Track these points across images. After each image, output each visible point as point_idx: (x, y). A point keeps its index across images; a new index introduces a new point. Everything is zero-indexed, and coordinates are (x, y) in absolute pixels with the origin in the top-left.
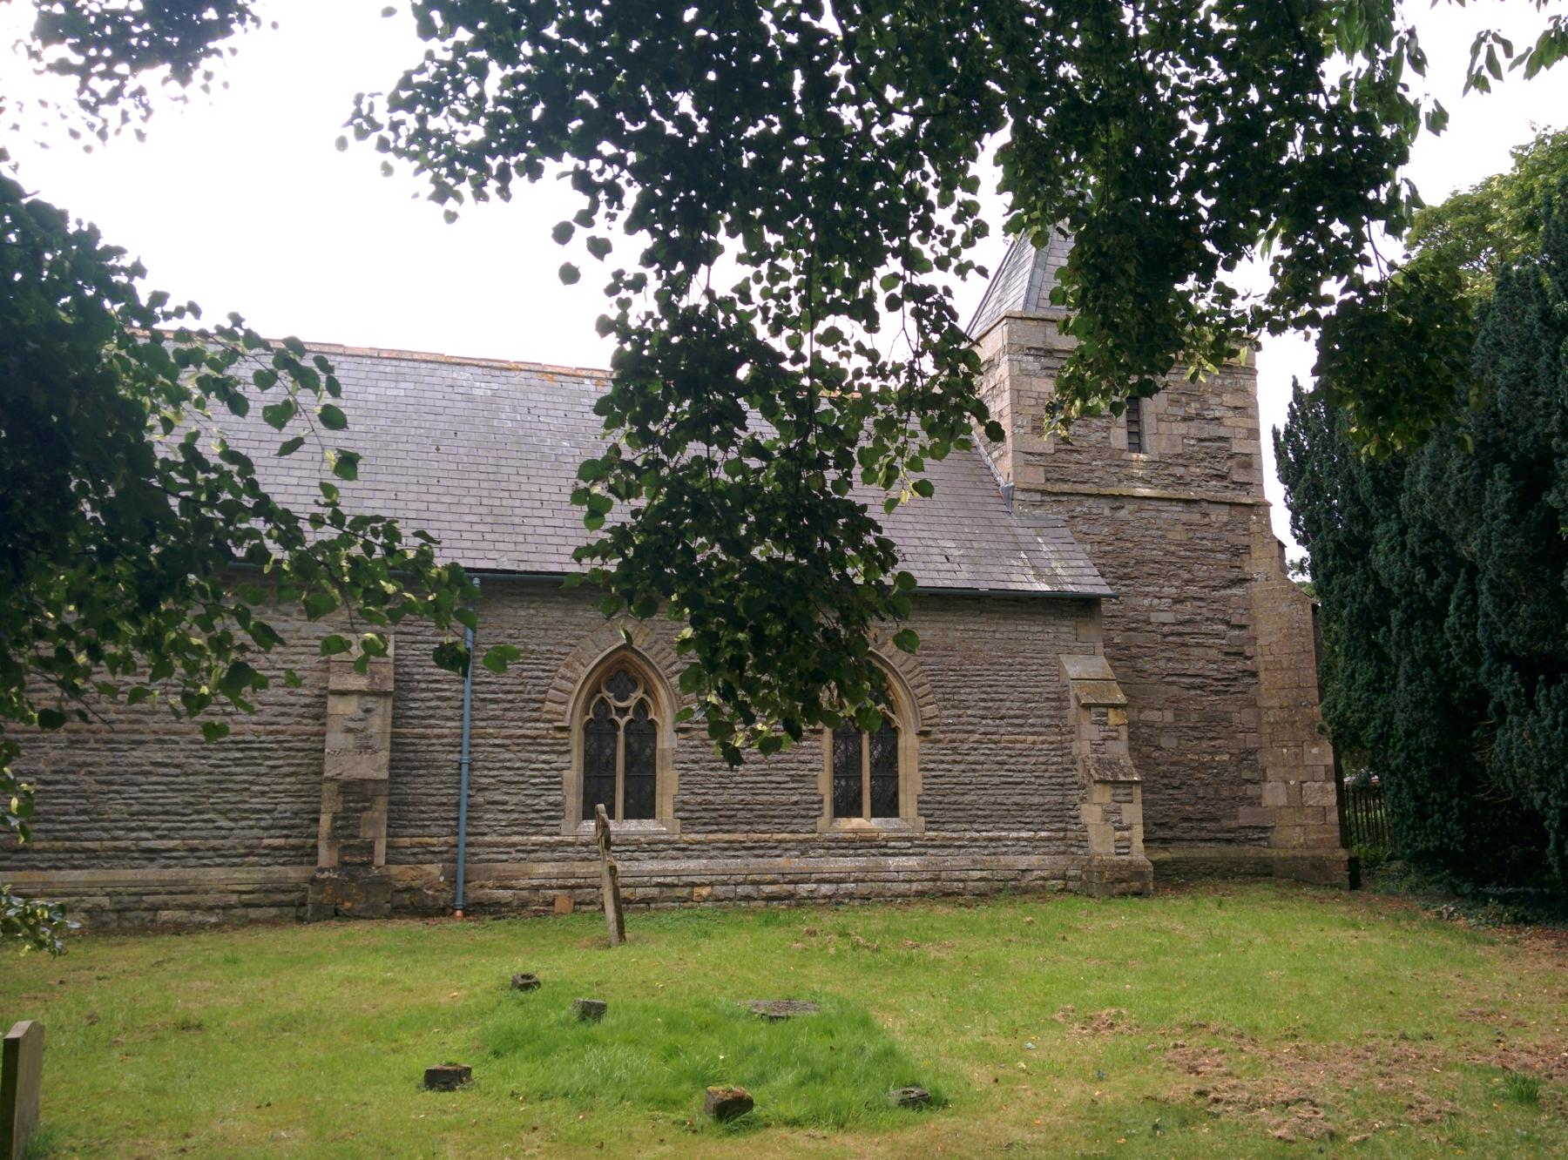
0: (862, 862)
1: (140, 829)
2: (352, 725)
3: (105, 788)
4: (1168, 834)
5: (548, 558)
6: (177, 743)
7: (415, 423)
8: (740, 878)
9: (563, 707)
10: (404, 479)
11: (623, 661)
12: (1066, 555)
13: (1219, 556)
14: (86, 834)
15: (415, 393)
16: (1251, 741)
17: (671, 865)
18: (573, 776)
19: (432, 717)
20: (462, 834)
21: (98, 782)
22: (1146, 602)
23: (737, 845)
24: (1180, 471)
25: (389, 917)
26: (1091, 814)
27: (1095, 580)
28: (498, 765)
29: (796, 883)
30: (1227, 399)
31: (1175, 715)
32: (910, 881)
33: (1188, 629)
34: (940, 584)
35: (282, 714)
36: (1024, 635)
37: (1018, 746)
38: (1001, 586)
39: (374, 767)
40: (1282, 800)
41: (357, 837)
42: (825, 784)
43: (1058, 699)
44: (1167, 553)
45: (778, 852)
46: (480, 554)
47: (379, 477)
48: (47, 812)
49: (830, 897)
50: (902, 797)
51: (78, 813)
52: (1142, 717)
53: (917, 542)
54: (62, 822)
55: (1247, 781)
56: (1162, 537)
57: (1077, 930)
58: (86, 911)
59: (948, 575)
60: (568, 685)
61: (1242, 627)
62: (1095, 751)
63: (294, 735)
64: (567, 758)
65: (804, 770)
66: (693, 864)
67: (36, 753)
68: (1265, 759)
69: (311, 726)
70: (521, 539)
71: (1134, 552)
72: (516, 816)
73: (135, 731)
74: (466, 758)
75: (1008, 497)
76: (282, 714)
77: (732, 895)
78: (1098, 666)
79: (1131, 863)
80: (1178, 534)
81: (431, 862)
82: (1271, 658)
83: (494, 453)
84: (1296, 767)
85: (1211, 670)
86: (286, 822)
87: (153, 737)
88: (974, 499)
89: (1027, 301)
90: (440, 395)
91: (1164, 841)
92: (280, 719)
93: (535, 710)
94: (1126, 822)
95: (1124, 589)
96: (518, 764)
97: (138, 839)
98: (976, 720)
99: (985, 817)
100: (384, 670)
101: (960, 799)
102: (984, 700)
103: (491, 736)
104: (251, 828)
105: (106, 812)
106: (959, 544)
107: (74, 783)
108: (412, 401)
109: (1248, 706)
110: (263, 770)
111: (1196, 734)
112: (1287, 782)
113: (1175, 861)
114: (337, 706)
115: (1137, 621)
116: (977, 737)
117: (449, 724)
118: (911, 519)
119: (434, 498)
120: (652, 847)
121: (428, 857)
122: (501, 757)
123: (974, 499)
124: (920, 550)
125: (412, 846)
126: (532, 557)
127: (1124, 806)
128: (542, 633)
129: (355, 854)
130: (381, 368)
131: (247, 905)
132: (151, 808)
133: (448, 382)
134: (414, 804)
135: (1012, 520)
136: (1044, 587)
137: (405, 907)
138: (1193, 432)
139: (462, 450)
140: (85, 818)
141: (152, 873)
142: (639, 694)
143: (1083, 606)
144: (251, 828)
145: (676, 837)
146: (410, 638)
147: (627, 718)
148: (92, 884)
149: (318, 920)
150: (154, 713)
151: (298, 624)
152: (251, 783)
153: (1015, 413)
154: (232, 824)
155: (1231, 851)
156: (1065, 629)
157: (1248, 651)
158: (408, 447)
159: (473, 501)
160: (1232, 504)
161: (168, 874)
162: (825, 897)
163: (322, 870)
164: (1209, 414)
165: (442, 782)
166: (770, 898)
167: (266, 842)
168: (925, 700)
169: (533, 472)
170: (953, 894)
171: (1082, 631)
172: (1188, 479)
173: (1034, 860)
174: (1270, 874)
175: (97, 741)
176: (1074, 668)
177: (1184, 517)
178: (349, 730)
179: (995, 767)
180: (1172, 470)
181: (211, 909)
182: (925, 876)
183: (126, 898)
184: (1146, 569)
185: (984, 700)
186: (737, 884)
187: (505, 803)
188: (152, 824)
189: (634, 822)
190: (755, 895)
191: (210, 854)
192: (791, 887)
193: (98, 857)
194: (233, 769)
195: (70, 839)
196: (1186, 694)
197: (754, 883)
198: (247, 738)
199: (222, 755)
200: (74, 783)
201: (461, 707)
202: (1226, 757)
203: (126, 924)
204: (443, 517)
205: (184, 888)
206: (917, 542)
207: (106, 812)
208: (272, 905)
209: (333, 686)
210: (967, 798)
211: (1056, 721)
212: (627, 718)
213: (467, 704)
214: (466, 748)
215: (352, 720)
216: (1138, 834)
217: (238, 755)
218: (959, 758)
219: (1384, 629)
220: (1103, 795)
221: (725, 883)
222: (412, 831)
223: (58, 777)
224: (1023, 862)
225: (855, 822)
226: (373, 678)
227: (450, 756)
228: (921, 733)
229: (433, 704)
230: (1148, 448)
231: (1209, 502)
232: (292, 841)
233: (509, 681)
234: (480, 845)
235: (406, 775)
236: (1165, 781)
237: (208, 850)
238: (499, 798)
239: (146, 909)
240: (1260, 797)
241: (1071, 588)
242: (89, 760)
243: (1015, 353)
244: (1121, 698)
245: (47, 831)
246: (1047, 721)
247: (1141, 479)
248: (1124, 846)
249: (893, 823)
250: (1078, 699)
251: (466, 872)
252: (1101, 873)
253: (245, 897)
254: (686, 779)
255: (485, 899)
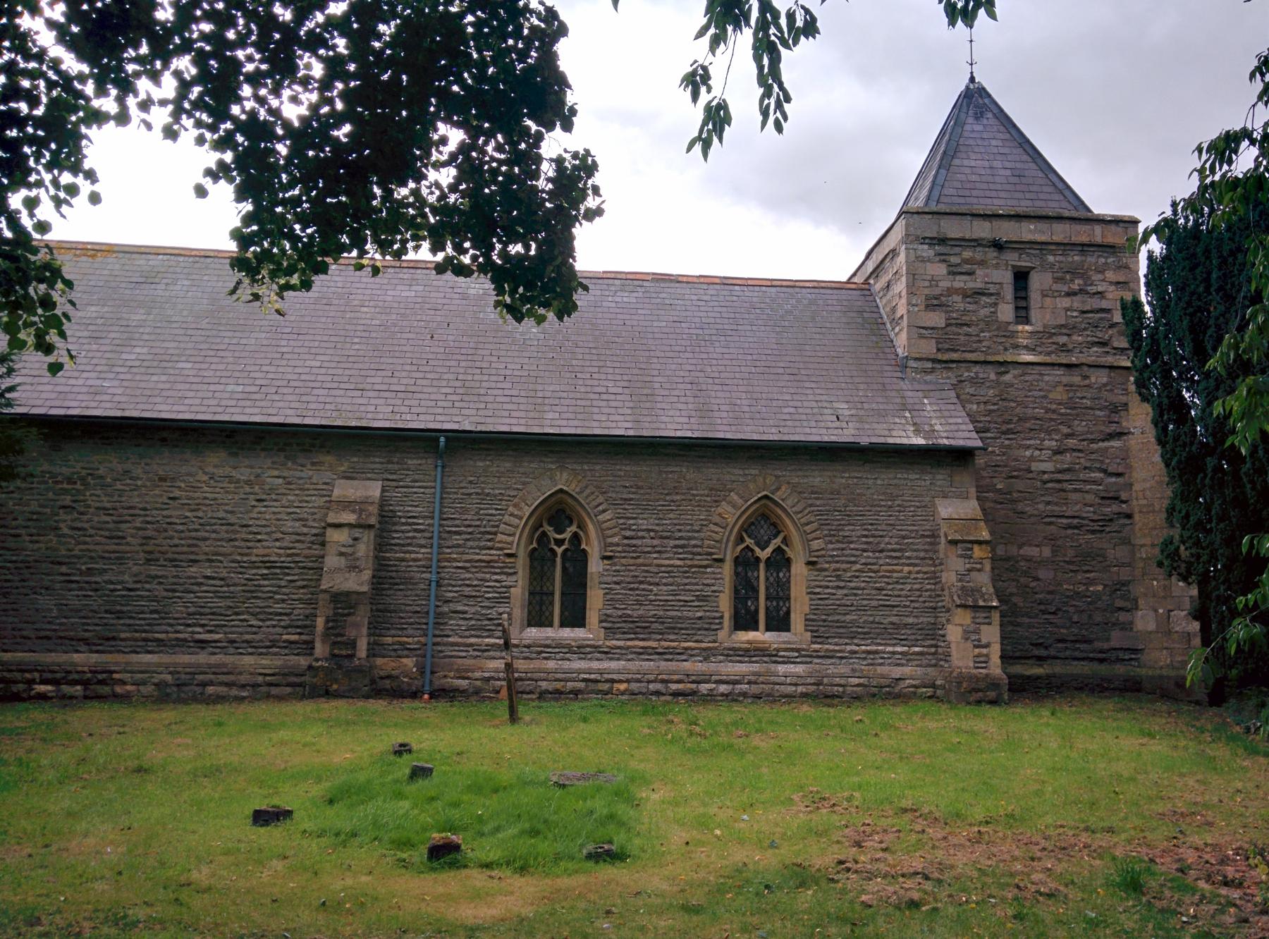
0: (756, 667)
1: (195, 625)
2: (343, 550)
3: (170, 594)
4: (1043, 652)
5: (500, 420)
6: (221, 562)
7: (419, 318)
8: (652, 677)
9: (511, 539)
10: (401, 361)
11: (561, 502)
12: (946, 414)
13: (1098, 413)
14: (157, 628)
15: (423, 294)
16: (1124, 574)
17: (595, 665)
18: (519, 590)
19: (409, 545)
20: (430, 634)
21: (167, 590)
22: (1028, 453)
23: (650, 651)
24: (1063, 339)
25: (367, 697)
26: (953, 633)
27: (967, 435)
28: (460, 582)
29: (699, 683)
30: (1110, 275)
31: (1053, 551)
32: (796, 685)
33: (1067, 477)
34: (826, 439)
35: (298, 541)
36: (902, 482)
37: (895, 575)
38: (882, 440)
39: (358, 582)
40: (1152, 626)
41: (342, 635)
42: (725, 604)
43: (933, 536)
44: (1047, 411)
45: (684, 657)
46: (448, 418)
47: (382, 360)
48: (130, 612)
49: (727, 695)
50: (793, 615)
51: (152, 612)
52: (1021, 552)
53: (814, 404)
54: (140, 619)
55: (1120, 609)
56: (1045, 397)
57: (897, 729)
58: (155, 685)
59: (836, 432)
60: (515, 521)
61: (1119, 475)
62: (960, 580)
63: (307, 557)
64: (514, 578)
65: (708, 591)
66: (614, 665)
67: (122, 568)
68: (1137, 590)
69: (317, 551)
70: (483, 406)
71: (1018, 410)
72: (473, 622)
73: (192, 553)
74: (434, 577)
75: (903, 366)
76: (298, 541)
77: (644, 690)
78: (970, 508)
79: (987, 675)
80: (1059, 394)
81: (407, 657)
82: (1145, 502)
83: (475, 339)
84: (1164, 597)
85: (1088, 512)
86: (300, 623)
87: (204, 557)
88: (874, 368)
89: (928, 198)
90: (442, 295)
91: (1040, 658)
92: (296, 545)
93: (489, 540)
94: (984, 641)
95: (1007, 442)
96: (475, 583)
97: (193, 633)
98: (858, 553)
99: (865, 633)
100: (371, 508)
101: (842, 618)
102: (866, 536)
103: (455, 560)
104: (274, 626)
105: (171, 612)
106: (851, 405)
107: (149, 590)
108: (420, 300)
109: (1123, 543)
110: (283, 583)
111: (1071, 567)
112: (1156, 611)
113: (1048, 676)
114: (335, 536)
115: (1019, 470)
116: (858, 566)
117: (423, 550)
118: (813, 385)
119: (421, 375)
120: (580, 650)
121: (406, 652)
122: (462, 576)
123: (874, 368)
124: (815, 411)
125: (393, 644)
126: (489, 420)
127: (983, 627)
128: (496, 480)
129: (342, 647)
130: (401, 276)
131: (270, 685)
132: (202, 610)
133: (450, 284)
134: (395, 611)
135: (904, 385)
136: (921, 441)
137: (387, 690)
138: (1076, 305)
139: (450, 338)
140: (156, 616)
141: (202, 658)
142: (574, 528)
143: (959, 457)
144: (274, 626)
145: (601, 643)
146: (394, 484)
147: (563, 547)
148: (159, 665)
149: (313, 698)
150: (205, 539)
151: (311, 473)
152: (275, 593)
153: (911, 293)
154: (261, 624)
155: (1103, 669)
156: (941, 477)
157: (1124, 496)
158: (411, 336)
159: (451, 377)
160: (1111, 368)
161: (214, 659)
162: (722, 695)
163: (317, 660)
164: (1092, 289)
165: (417, 595)
166: (676, 694)
167: (285, 637)
168: (813, 535)
169: (503, 353)
170: (833, 696)
171: (957, 478)
172: (1070, 347)
173: (907, 670)
174: (1138, 690)
175: (165, 560)
176: (946, 509)
177: (1065, 380)
178: (341, 554)
179: (874, 592)
180: (1055, 339)
181: (243, 686)
182: (809, 680)
183: (183, 676)
184: (1028, 425)
185: (866, 536)
186: (649, 682)
187: (465, 612)
188: (203, 622)
189: (534, 630)
190: (664, 691)
191: (245, 645)
192: (694, 686)
193: (165, 646)
194: (262, 582)
195: (145, 631)
196: (1063, 533)
197: (663, 681)
198: (272, 559)
199: (254, 571)
200: (149, 590)
201: (431, 538)
202: (1100, 588)
203: (183, 695)
204: (425, 390)
205: (225, 670)
206: (814, 404)
207: (171, 612)
208: (288, 685)
209: (330, 520)
210: (848, 618)
211: (930, 555)
212: (563, 547)
213: (436, 534)
214: (434, 569)
215: (344, 546)
216: (995, 652)
217: (265, 571)
218: (842, 584)
219: (1202, 475)
220: (963, 618)
221: (639, 681)
222: (393, 632)
223: (139, 586)
224: (897, 672)
225: (752, 635)
226: (361, 514)
227: (423, 575)
228: (809, 563)
229: (410, 534)
230: (1033, 320)
231: (1090, 366)
232: (304, 637)
233: (469, 517)
234: (445, 645)
235: (390, 589)
236: (1042, 607)
237: (243, 642)
238: (460, 608)
239: (197, 685)
240: (1131, 623)
241: (946, 442)
242: (160, 573)
243: (911, 242)
244: (985, 535)
245: (130, 625)
246: (922, 554)
247: (1026, 347)
248: (983, 661)
249: (784, 636)
250: (946, 536)
251: (433, 664)
252: (959, 684)
253: (268, 678)
254: (609, 597)
255: (447, 687)
